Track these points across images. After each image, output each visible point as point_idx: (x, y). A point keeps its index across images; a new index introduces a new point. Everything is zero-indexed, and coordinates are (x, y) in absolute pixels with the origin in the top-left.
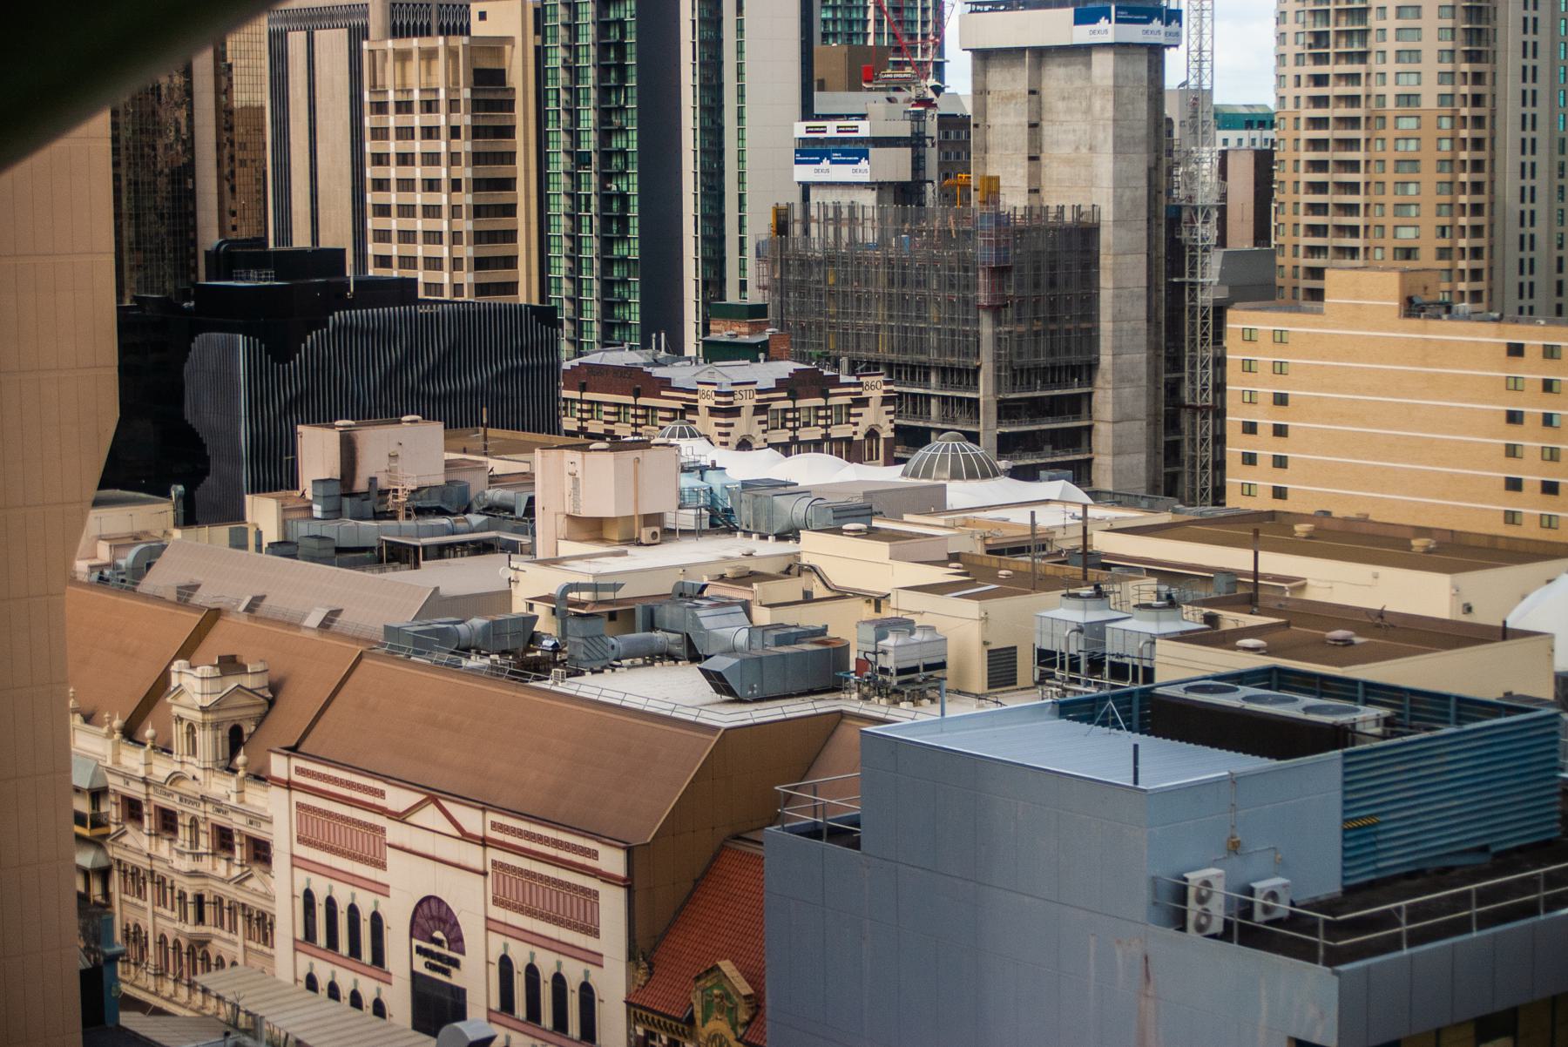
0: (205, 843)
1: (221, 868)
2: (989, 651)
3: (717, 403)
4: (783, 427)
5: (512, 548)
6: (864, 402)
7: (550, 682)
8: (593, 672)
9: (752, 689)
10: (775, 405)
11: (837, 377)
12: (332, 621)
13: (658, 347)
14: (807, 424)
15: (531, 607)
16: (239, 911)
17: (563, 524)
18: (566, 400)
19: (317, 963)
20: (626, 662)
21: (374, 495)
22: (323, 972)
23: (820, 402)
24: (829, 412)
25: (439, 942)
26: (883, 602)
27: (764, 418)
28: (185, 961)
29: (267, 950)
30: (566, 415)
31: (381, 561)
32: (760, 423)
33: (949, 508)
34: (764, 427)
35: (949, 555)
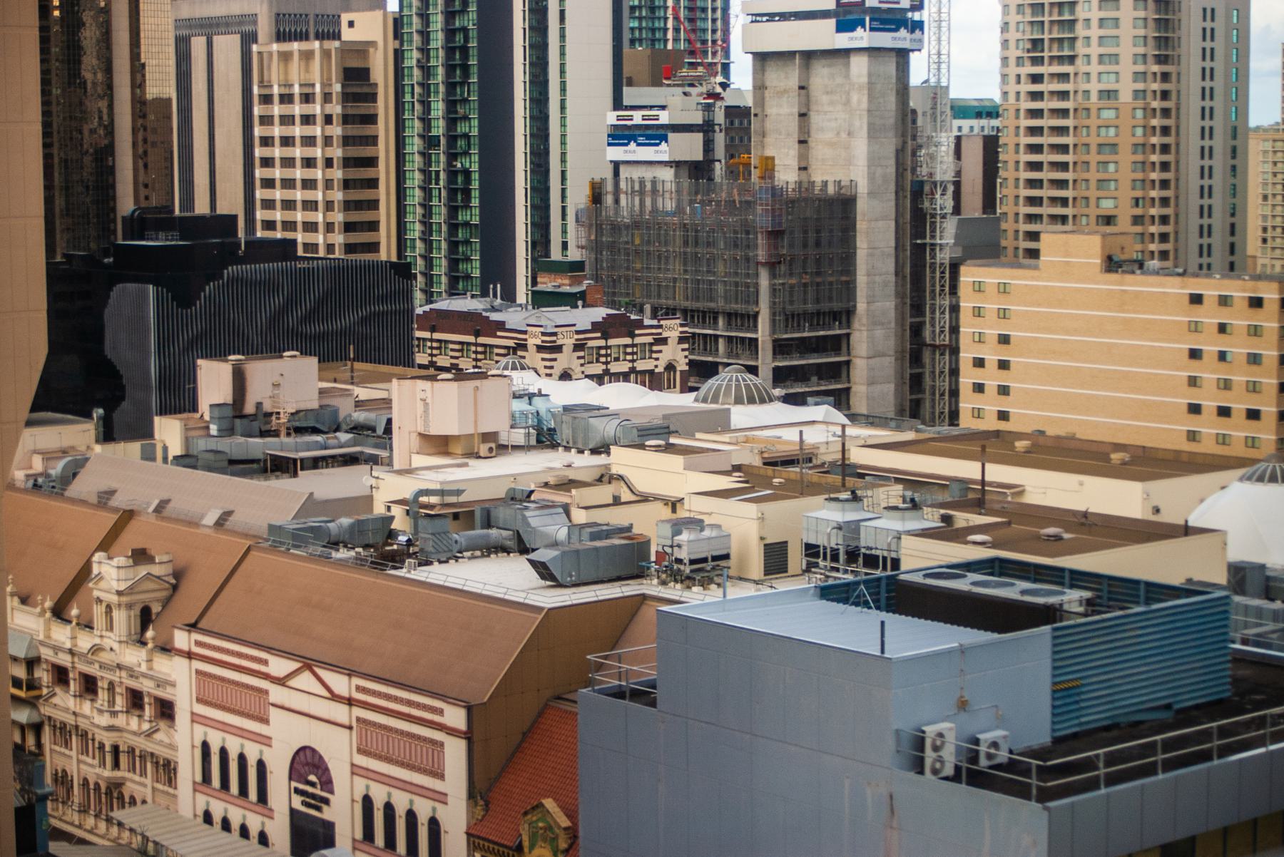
0: (120, 703)
1: (134, 723)
2: (765, 545)
3: (543, 341)
4: (598, 361)
5: (374, 460)
6: (664, 341)
7: (404, 570)
8: (440, 562)
9: (571, 576)
10: (591, 344)
11: (642, 321)
12: (226, 520)
13: (495, 296)
14: (617, 359)
15: (389, 508)
16: (149, 759)
17: (415, 441)
18: (418, 339)
19: (213, 801)
20: (467, 554)
21: (261, 417)
22: (218, 809)
23: (628, 341)
24: (635, 349)
25: (313, 784)
26: (678, 505)
27: (581, 354)
28: (103, 800)
29: (171, 791)
30: (419, 352)
31: (265, 471)
32: (579, 358)
33: (733, 428)
34: (582, 361)
35: (733, 466)
